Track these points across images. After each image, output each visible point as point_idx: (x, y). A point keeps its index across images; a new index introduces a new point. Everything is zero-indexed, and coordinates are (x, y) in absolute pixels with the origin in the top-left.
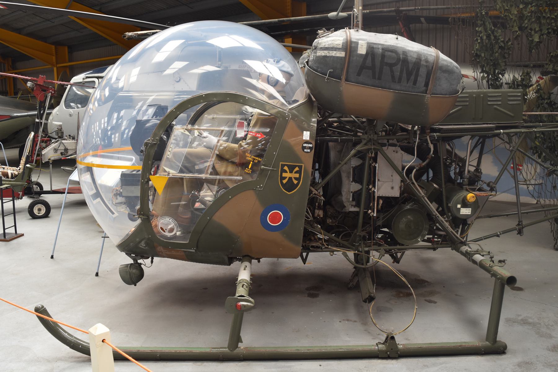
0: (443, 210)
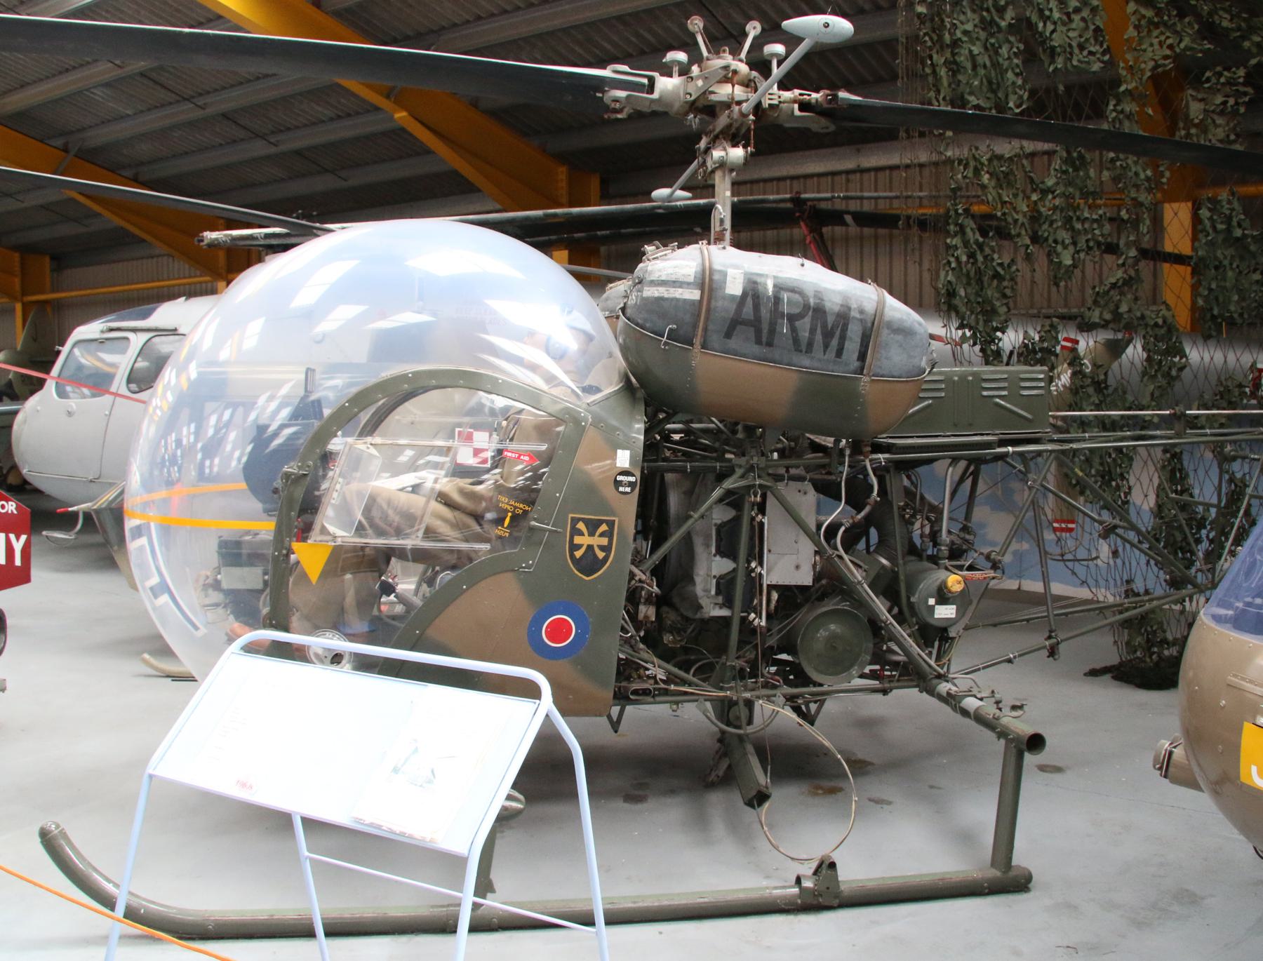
0: (901, 612)
